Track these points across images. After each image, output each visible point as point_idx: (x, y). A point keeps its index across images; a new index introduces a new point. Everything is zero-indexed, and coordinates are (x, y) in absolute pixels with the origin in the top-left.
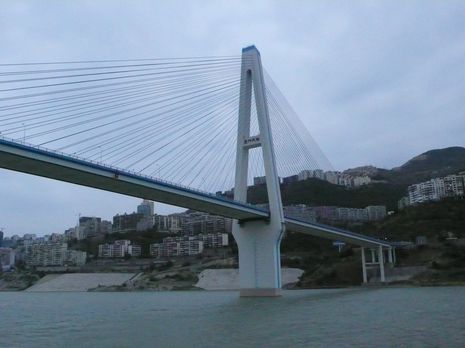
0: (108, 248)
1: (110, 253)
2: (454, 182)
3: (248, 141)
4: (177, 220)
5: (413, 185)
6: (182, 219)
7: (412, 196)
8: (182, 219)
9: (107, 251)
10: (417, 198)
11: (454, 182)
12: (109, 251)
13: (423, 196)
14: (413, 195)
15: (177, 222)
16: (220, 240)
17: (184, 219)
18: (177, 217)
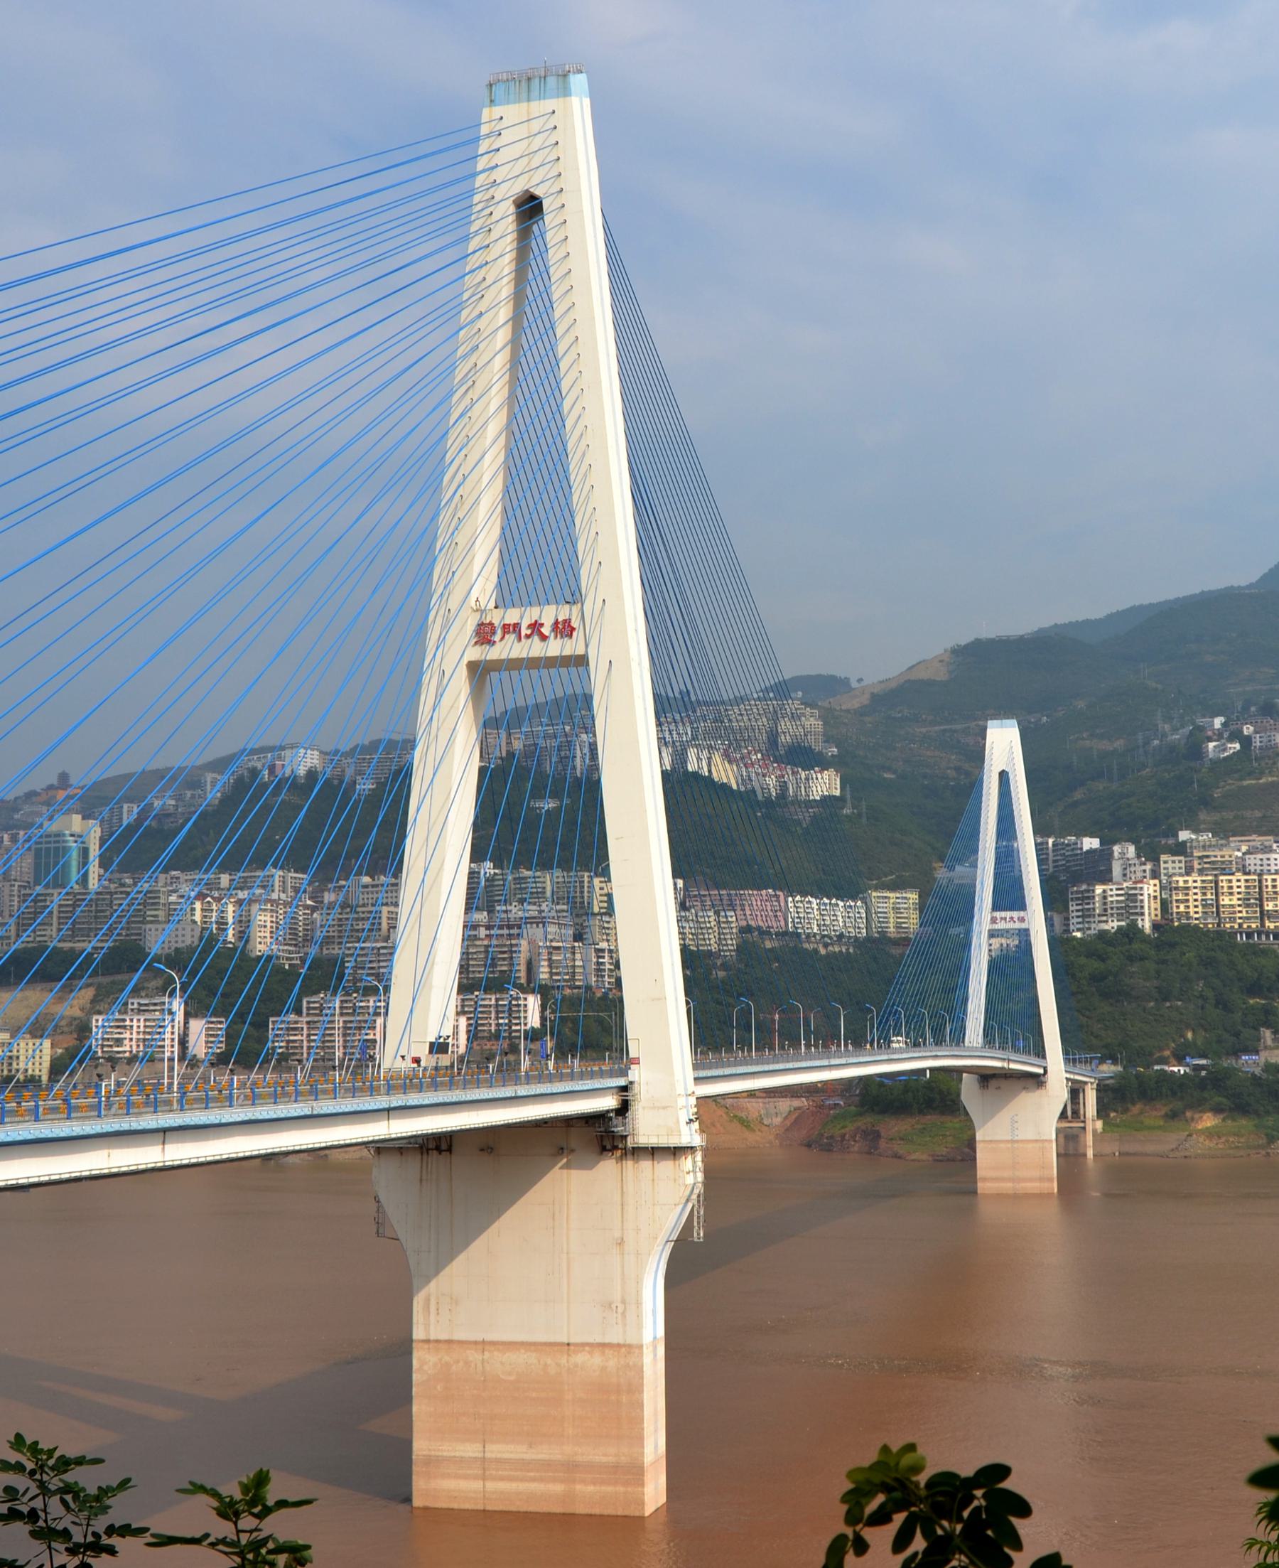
0: (124, 1027)
1: (134, 1043)
2: (1195, 891)
3: (999, 920)
4: (269, 915)
5: (1084, 887)
6: (281, 912)
7: (1078, 917)
8: (281, 912)
9: (122, 1036)
10: (1093, 926)
11: (1195, 891)
12: (127, 1035)
13: (1113, 921)
14: (1080, 914)
15: (268, 924)
16: (513, 1011)
17: (285, 913)
18: (272, 906)
